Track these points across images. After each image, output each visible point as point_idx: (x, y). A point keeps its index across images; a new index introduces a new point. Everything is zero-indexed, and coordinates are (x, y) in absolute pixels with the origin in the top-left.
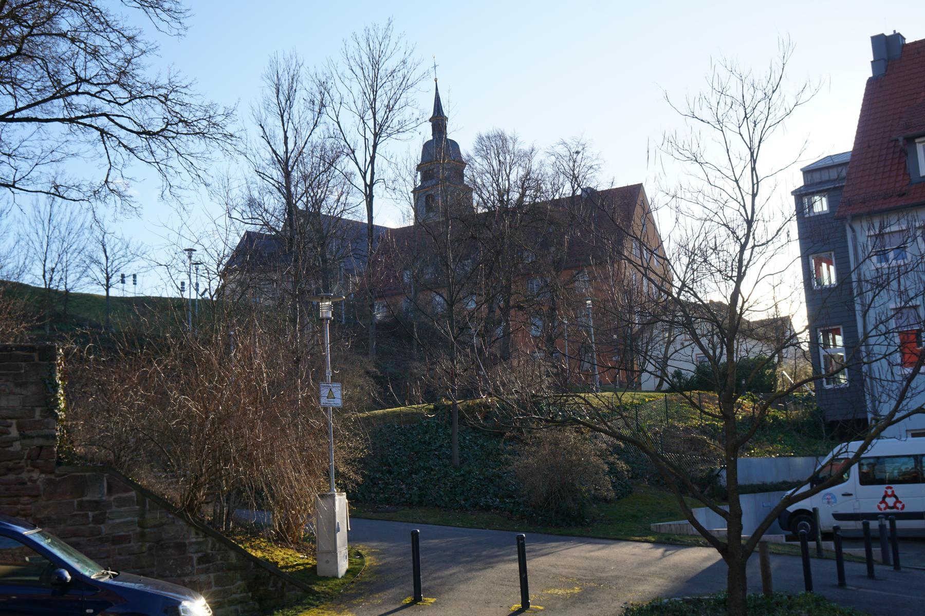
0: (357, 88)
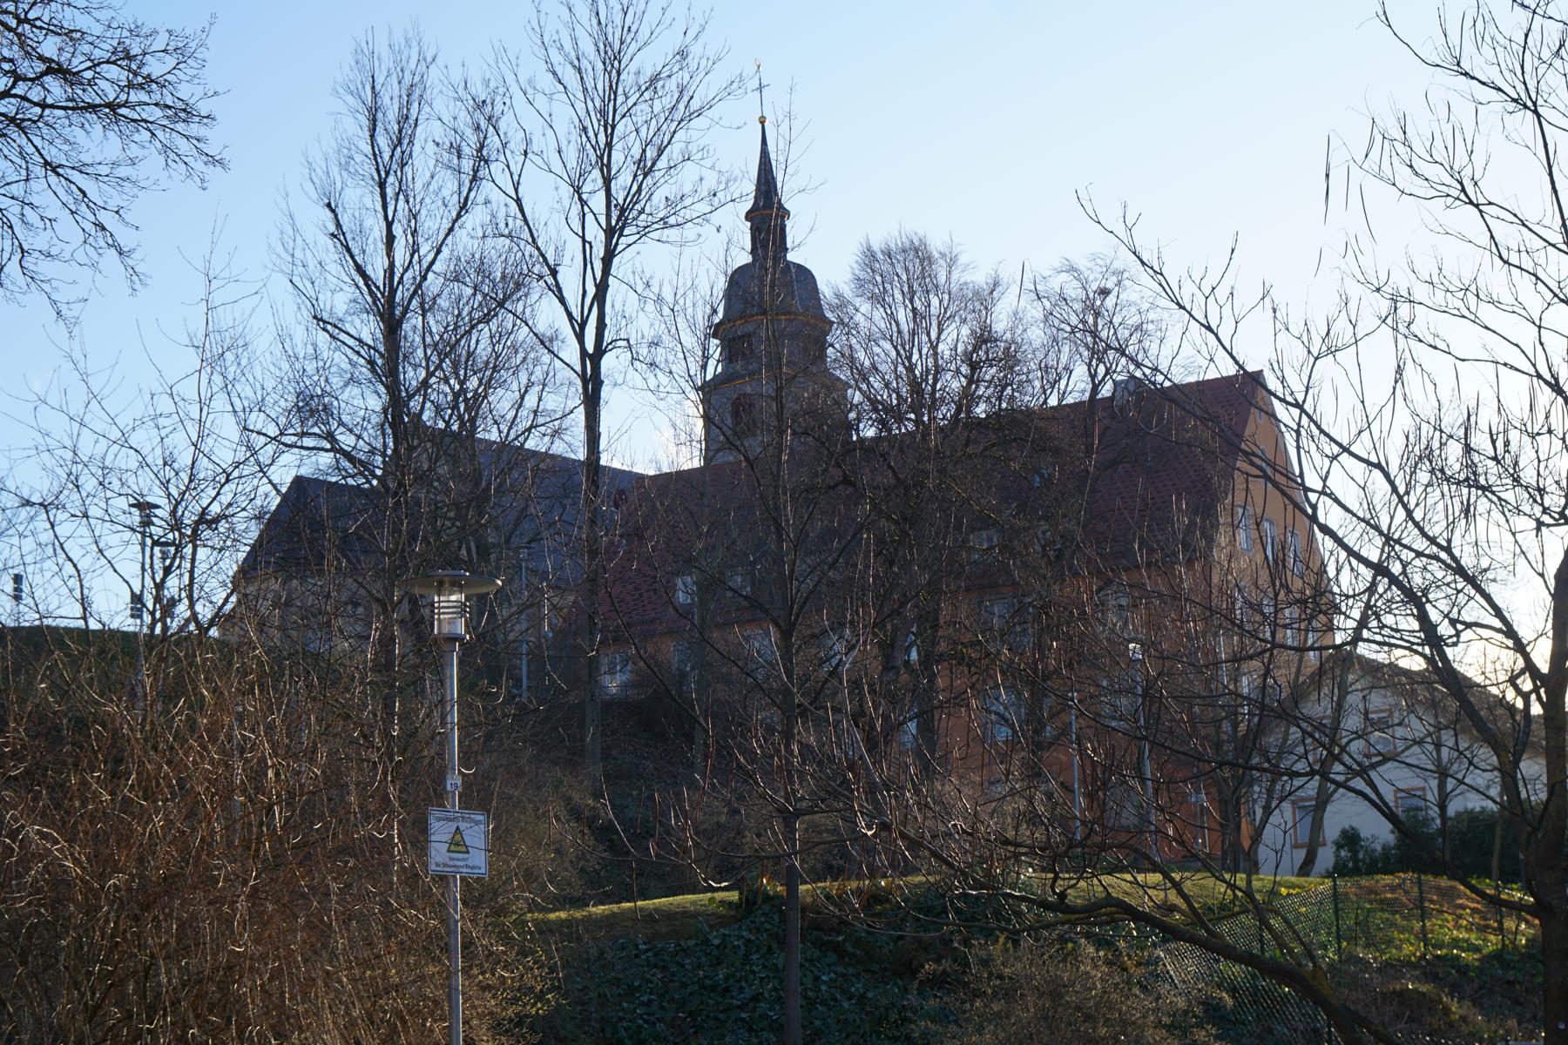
0: (565, 117)
